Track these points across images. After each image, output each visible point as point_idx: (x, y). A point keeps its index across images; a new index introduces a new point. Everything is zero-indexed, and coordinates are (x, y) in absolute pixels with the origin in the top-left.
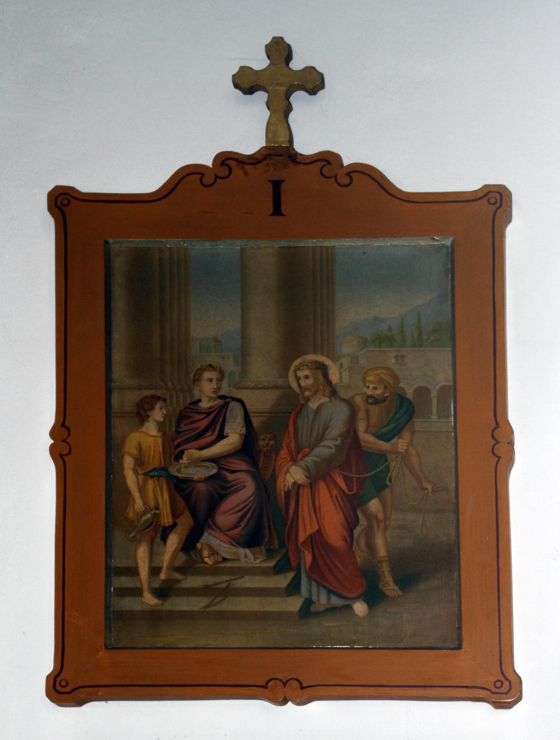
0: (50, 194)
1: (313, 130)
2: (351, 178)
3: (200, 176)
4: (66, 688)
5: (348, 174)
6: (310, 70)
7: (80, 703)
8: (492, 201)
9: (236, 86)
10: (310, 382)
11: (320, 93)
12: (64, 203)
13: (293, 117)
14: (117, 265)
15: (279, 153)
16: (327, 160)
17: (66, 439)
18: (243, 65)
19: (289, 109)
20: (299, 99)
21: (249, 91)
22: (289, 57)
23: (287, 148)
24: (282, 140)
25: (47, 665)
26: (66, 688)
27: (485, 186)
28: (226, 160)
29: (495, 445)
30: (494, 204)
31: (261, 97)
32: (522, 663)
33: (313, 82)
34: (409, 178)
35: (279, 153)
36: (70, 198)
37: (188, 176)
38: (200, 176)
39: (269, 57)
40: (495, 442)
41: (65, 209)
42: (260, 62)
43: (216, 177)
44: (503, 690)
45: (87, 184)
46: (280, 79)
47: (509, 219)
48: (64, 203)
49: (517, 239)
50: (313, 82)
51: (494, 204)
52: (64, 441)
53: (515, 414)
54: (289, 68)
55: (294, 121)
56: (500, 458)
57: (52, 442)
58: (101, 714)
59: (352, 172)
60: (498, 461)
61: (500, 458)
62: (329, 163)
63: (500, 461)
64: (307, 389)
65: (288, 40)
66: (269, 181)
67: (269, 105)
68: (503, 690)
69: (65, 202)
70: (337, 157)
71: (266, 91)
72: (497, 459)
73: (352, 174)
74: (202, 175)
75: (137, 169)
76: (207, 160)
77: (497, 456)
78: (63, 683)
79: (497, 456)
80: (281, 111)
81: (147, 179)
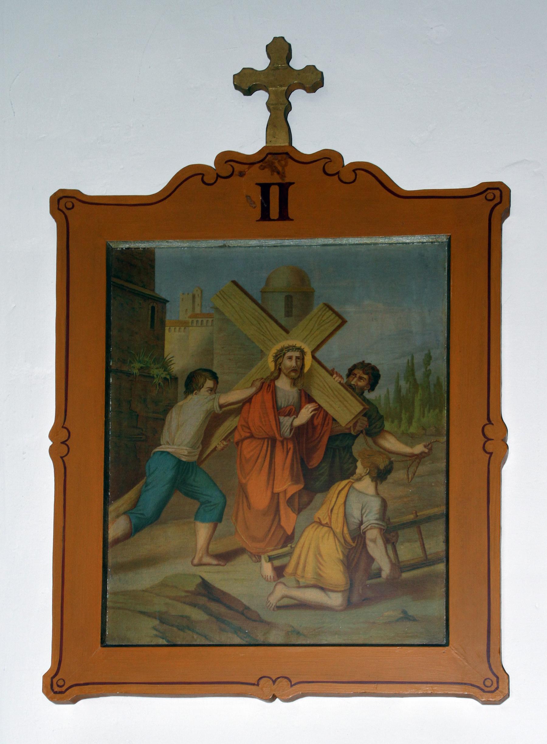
0: (52, 198)
1: (313, 129)
3: (200, 176)
4: (61, 686)
6: (311, 69)
7: (74, 701)
8: (490, 197)
9: (237, 87)
11: (320, 90)
13: (291, 117)
14: (113, 268)
15: (279, 155)
16: (328, 159)
17: (66, 441)
19: (288, 108)
20: (298, 98)
21: (248, 92)
22: (289, 57)
24: (282, 142)
25: (44, 662)
26: (61, 686)
28: (228, 159)
29: (486, 442)
30: (494, 200)
32: (511, 658)
33: (313, 80)
35: (279, 155)
38: (200, 176)
39: (269, 57)
41: (67, 212)
42: (261, 63)
43: (218, 176)
44: (491, 686)
45: (93, 187)
46: (280, 78)
47: (507, 213)
48: (65, 205)
49: (515, 234)
50: (313, 80)
51: (494, 200)
52: (63, 443)
53: (509, 412)
56: (258, 685)
57: (51, 443)
59: (357, 169)
60: (64, 424)
61: (258, 685)
63: (492, 458)
66: (292, 220)
67: (269, 105)
68: (491, 686)
69: (69, 205)
71: (267, 91)
72: (488, 455)
73: (356, 171)
74: (203, 175)
78: (61, 683)
80: (280, 112)
81: (148, 180)
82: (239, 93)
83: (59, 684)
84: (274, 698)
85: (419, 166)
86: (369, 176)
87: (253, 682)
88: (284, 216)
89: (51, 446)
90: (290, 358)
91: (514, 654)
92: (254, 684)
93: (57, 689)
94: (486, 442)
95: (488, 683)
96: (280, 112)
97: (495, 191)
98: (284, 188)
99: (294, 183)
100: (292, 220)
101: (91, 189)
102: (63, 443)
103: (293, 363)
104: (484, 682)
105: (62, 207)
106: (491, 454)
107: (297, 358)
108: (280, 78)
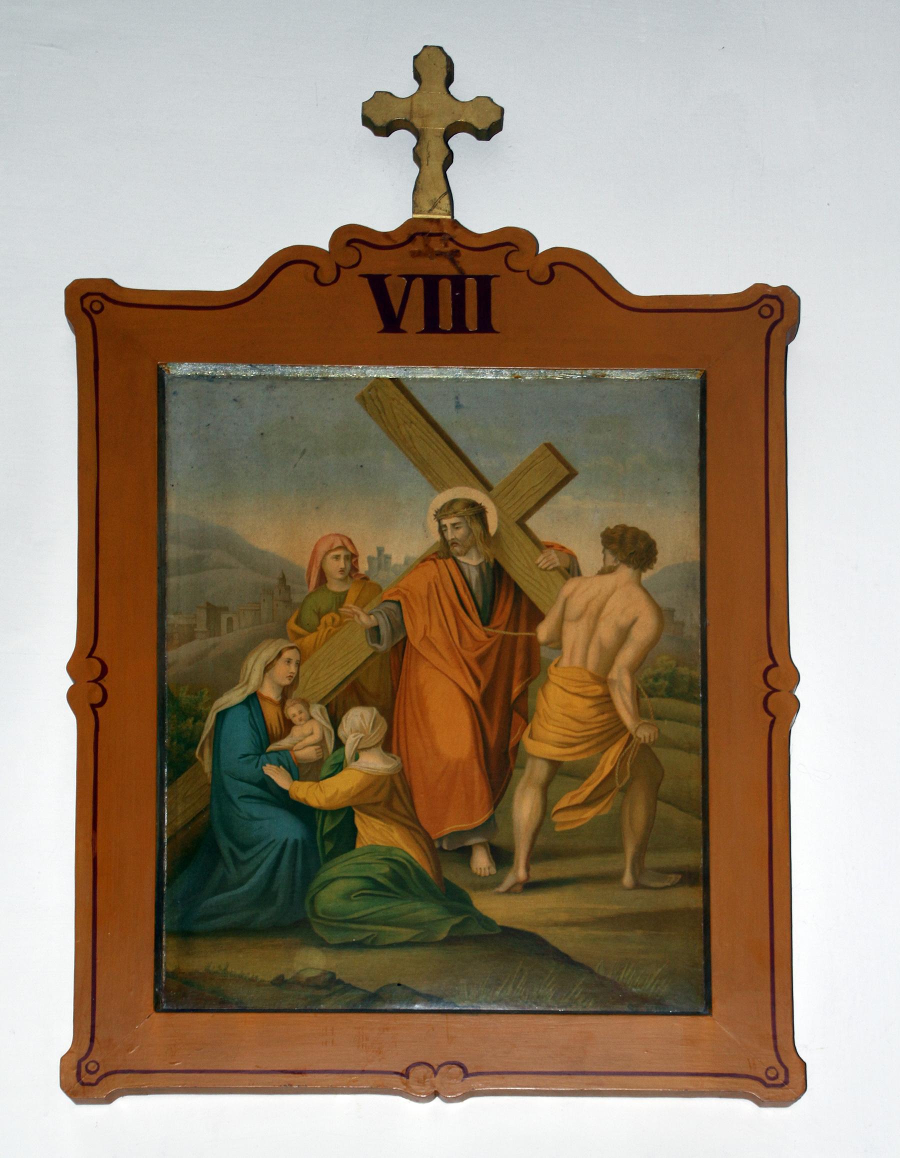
0: (786, 290)
1: (486, 198)
4: (90, 1075)
5: (551, 266)
7: (109, 1100)
9: (367, 121)
10: (460, 533)
12: (93, 306)
15: (432, 235)
16: (513, 242)
19: (449, 160)
21: (384, 130)
22: (449, 79)
23: (412, 233)
24: (439, 215)
25: (60, 1035)
26: (90, 1075)
27: (756, 287)
28: (352, 238)
29: (769, 694)
30: (771, 314)
31: (404, 139)
32: (809, 1035)
34: (644, 271)
37: (289, 262)
39: (417, 77)
41: (93, 315)
42: (404, 86)
44: (777, 1077)
46: (432, 114)
48: (93, 306)
49: (808, 363)
51: (771, 314)
52: (775, 690)
53: (805, 647)
54: (449, 93)
55: (175, 393)
58: (137, 1113)
64: (454, 543)
66: (497, 332)
68: (777, 1077)
69: (97, 307)
70: (532, 240)
78: (92, 1067)
81: (226, 270)
82: (368, 132)
83: (89, 1068)
85: (659, 257)
86: (576, 272)
87: (400, 1071)
88: (485, 325)
89: (71, 689)
90: (337, 557)
93: (86, 1078)
94: (769, 694)
95: (766, 311)
98: (484, 283)
99: (498, 276)
100: (497, 332)
101: (132, 279)
102: (775, 690)
103: (341, 564)
104: (766, 1073)
105: (87, 305)
108: (432, 114)
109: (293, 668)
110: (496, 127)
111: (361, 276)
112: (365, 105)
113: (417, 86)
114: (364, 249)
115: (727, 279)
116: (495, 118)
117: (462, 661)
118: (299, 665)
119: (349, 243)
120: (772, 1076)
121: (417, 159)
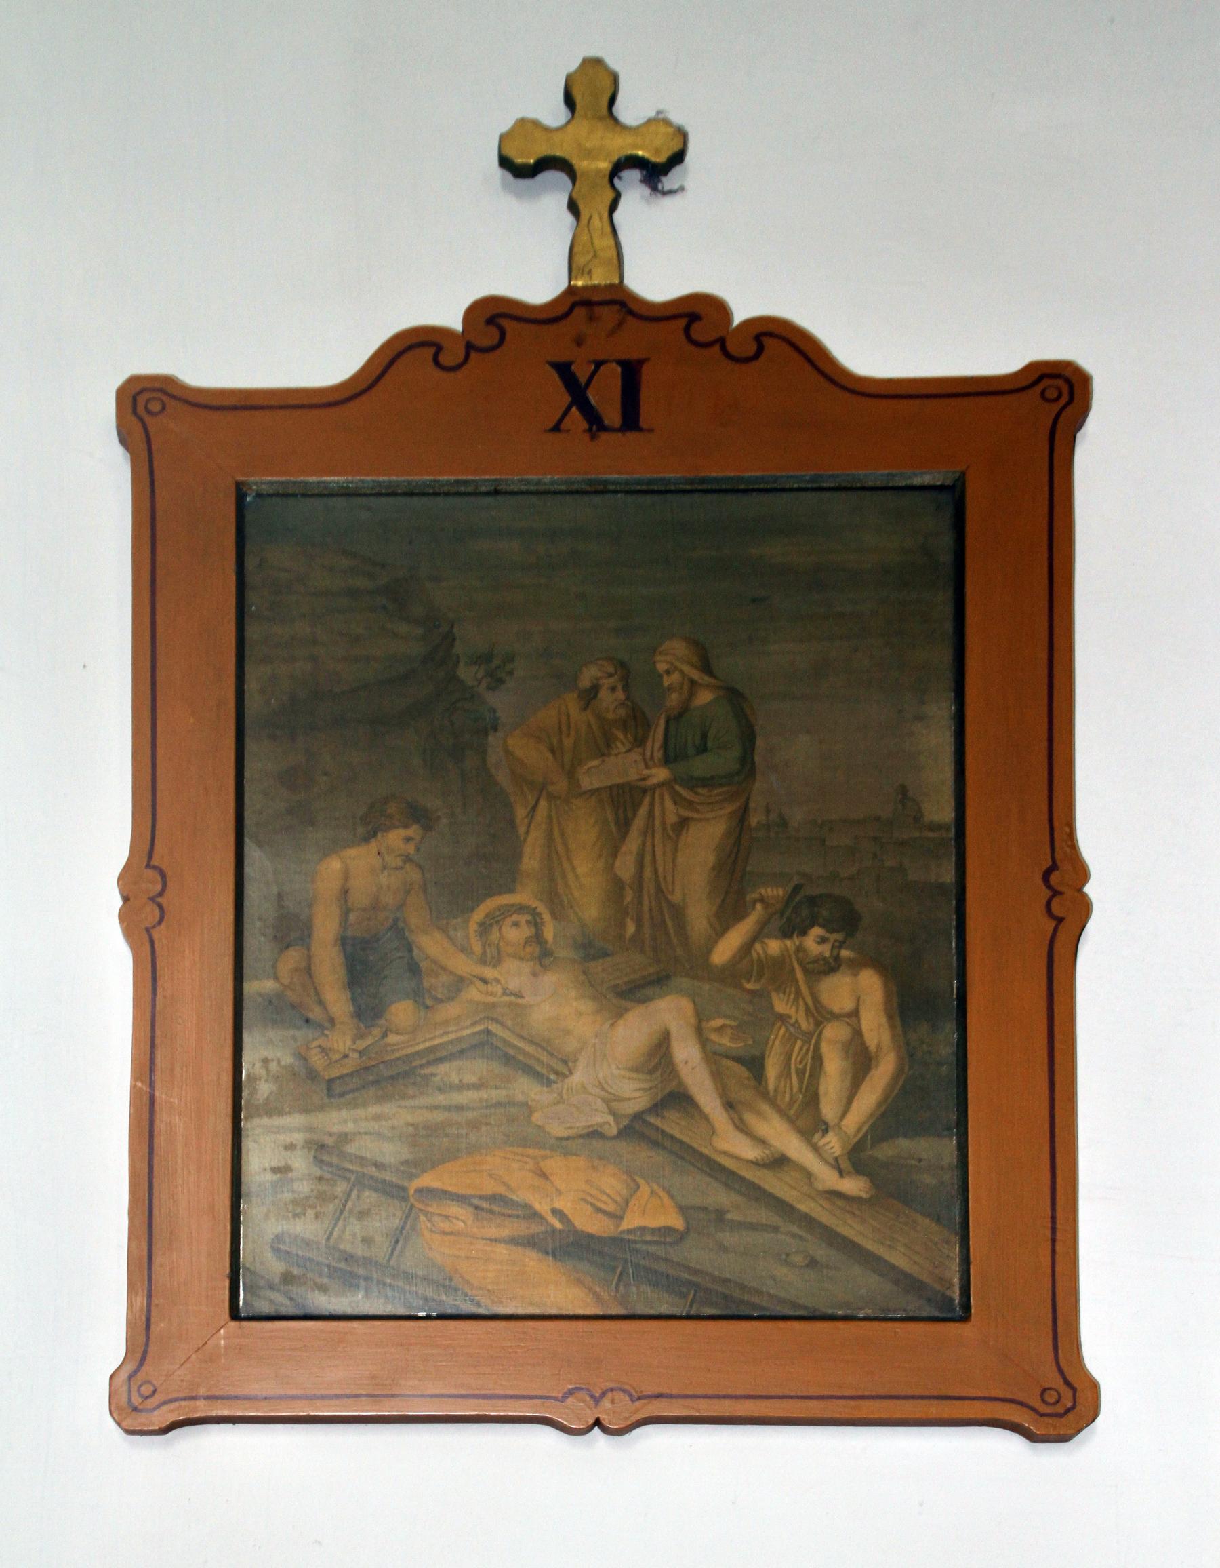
0: (121, 393)
1: (663, 255)
2: (760, 349)
5: (758, 338)
6: (660, 120)
9: (505, 162)
13: (617, 216)
15: (597, 305)
16: (697, 315)
18: (531, 115)
22: (612, 101)
23: (577, 304)
24: (600, 277)
27: (1032, 367)
28: (494, 316)
32: (1102, 1345)
34: (873, 348)
35: (597, 305)
36: (165, 398)
37: (413, 348)
39: (569, 101)
40: (159, 900)
42: (553, 113)
44: (1058, 394)
46: (598, 150)
56: (148, 866)
59: (770, 335)
60: (150, 856)
61: (148, 866)
62: (693, 318)
65: (612, 63)
68: (1054, 1402)
69: (155, 407)
72: (154, 862)
75: (296, 336)
76: (449, 316)
77: (155, 868)
79: (155, 868)
80: (593, 211)
81: (325, 356)
84: (597, 1422)
86: (783, 347)
90: (516, 924)
91: (1106, 1340)
92: (150, 856)
95: (1051, 1397)
96: (593, 211)
97: (1060, 382)
98: (631, 373)
106: (1060, 920)
107: (528, 922)
108: (598, 150)
109: (620, 695)
110: (678, 158)
111: (650, 430)
112: (502, 138)
113: (570, 115)
114: (505, 323)
115: (1000, 358)
116: (675, 146)
117: (396, 1253)
118: (626, 688)
119: (491, 321)
120: (1055, 395)
121: (573, 207)
